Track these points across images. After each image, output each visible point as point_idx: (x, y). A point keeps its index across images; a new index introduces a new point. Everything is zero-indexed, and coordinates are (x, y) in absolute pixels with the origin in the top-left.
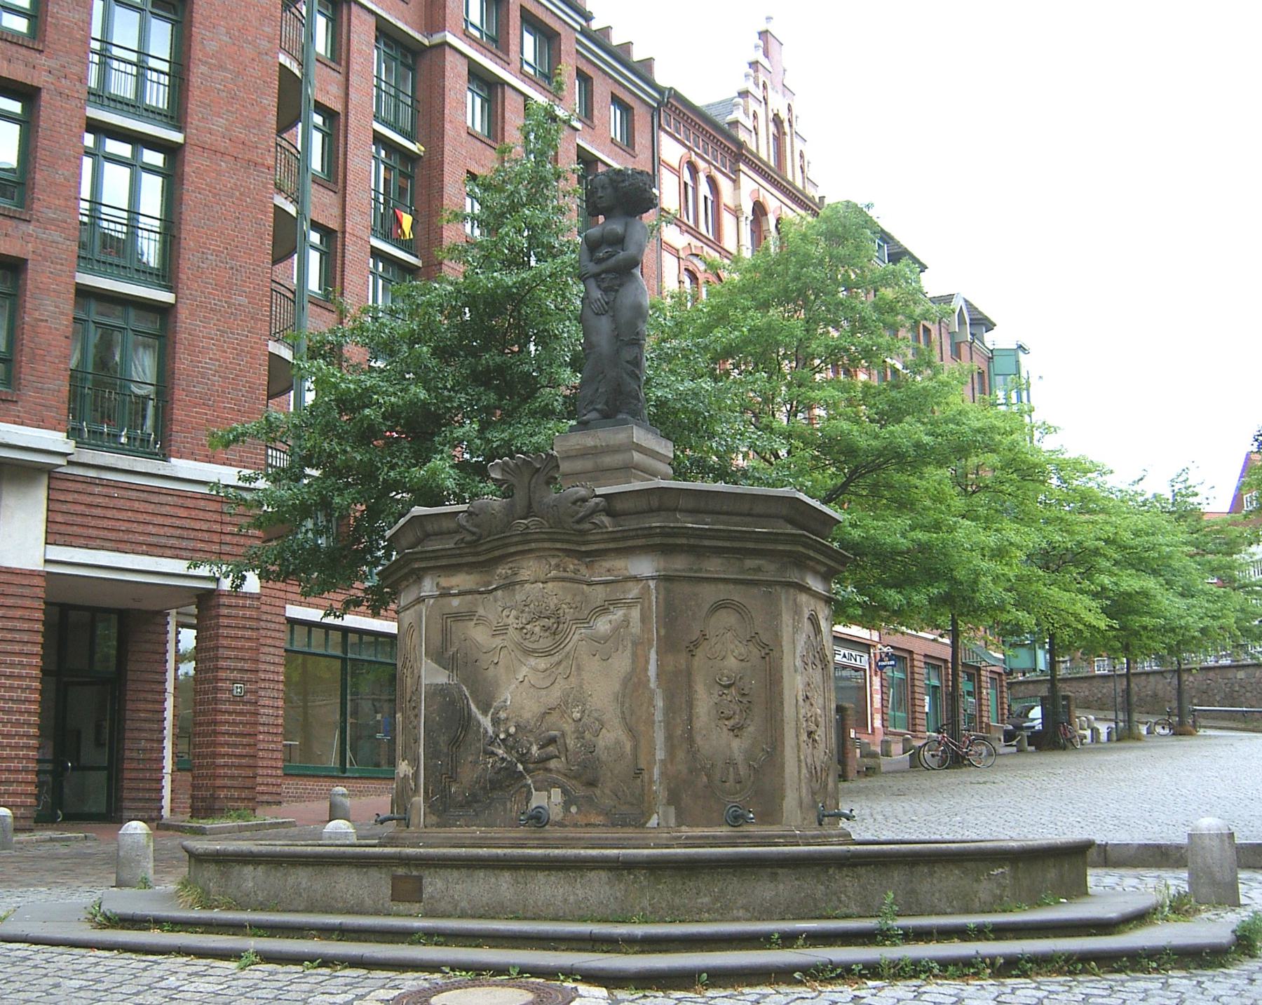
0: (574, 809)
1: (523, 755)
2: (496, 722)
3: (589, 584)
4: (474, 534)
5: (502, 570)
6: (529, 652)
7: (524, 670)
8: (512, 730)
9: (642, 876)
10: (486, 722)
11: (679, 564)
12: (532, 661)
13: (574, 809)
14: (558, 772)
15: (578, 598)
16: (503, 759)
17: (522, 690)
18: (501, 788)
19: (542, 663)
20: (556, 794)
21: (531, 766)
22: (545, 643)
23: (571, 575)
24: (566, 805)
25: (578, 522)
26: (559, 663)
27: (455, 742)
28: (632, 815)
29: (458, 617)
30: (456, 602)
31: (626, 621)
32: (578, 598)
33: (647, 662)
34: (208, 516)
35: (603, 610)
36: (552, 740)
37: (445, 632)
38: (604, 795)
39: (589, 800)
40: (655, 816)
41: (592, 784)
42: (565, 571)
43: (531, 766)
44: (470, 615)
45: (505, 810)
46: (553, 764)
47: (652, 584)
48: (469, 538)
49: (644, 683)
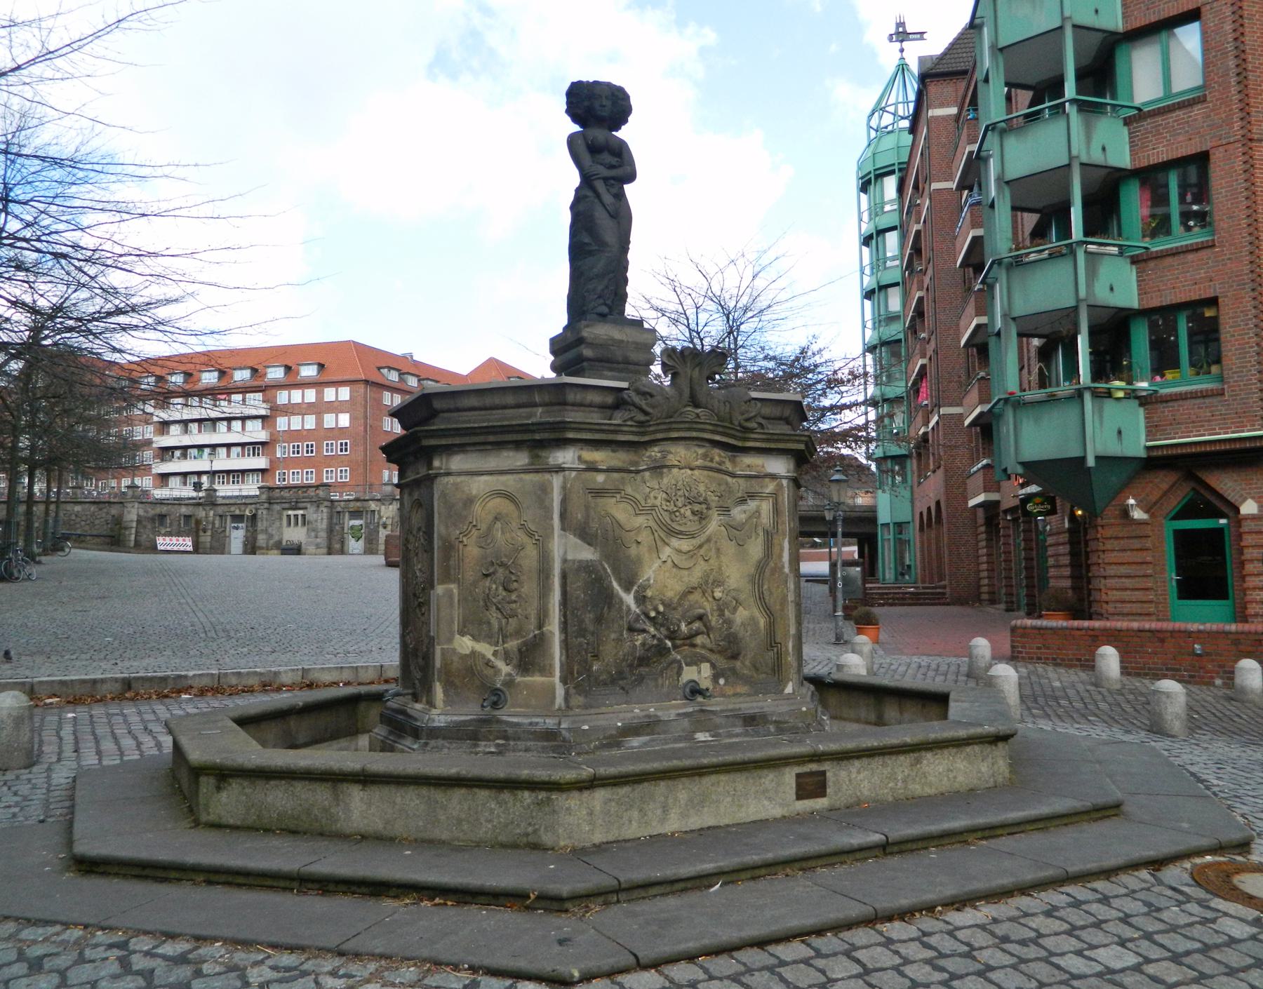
0: (722, 681)
1: (675, 632)
2: (641, 599)
3: (733, 475)
4: (646, 413)
5: (655, 452)
6: (672, 533)
7: (666, 552)
8: (661, 608)
10: (629, 599)
12: (675, 542)
13: (722, 681)
14: (703, 647)
15: (723, 488)
16: (654, 636)
17: (663, 572)
18: (648, 665)
19: (685, 545)
20: (706, 669)
21: (678, 642)
22: (692, 527)
23: (714, 465)
24: (715, 678)
25: (747, 420)
26: (700, 546)
27: (599, 620)
29: (599, 493)
30: (600, 478)
32: (723, 488)
33: (782, 550)
34: (1123, 570)
35: (743, 501)
36: (700, 618)
37: (587, 508)
39: (733, 670)
40: (790, 684)
41: (735, 657)
42: (712, 461)
43: (678, 642)
45: (657, 686)
46: (699, 640)
47: (785, 482)
48: (642, 418)
49: (778, 569)
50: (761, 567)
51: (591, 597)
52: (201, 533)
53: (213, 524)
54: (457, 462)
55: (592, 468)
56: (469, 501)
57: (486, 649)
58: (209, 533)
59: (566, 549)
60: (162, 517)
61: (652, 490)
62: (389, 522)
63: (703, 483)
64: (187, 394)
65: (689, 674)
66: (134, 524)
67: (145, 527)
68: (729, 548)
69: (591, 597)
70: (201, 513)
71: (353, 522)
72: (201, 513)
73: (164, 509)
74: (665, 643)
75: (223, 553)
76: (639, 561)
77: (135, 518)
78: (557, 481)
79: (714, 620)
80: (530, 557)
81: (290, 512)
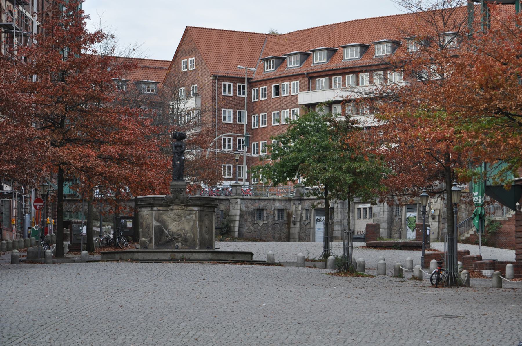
2: (168, 232)
5: (171, 207)
6: (175, 221)
9: (277, 261)
10: (166, 232)
11: (202, 208)
17: (173, 227)
19: (177, 223)
20: (180, 244)
22: (178, 219)
24: (182, 245)
27: (161, 235)
28: (194, 246)
29: (161, 214)
31: (192, 217)
35: (189, 215)
37: (159, 217)
38: (188, 244)
39: (186, 244)
44: (164, 214)
49: (195, 227)
50: (192, 226)
51: (160, 231)
52: (292, 225)
53: (301, 217)
54: (143, 209)
55: (159, 210)
56: (144, 216)
57: (146, 240)
58: (298, 225)
59: (155, 223)
60: (260, 211)
61: (171, 214)
62: (437, 213)
63: (180, 212)
64: (330, 74)
65: (177, 244)
66: (238, 218)
67: (246, 220)
68: (186, 224)
69: (160, 231)
70: (292, 207)
71: (409, 214)
72: (292, 207)
73: (261, 205)
74: (172, 239)
75: (308, 241)
76: (168, 225)
77: (238, 212)
78: (154, 212)
79: (182, 235)
80: (151, 226)
81: (361, 206)
